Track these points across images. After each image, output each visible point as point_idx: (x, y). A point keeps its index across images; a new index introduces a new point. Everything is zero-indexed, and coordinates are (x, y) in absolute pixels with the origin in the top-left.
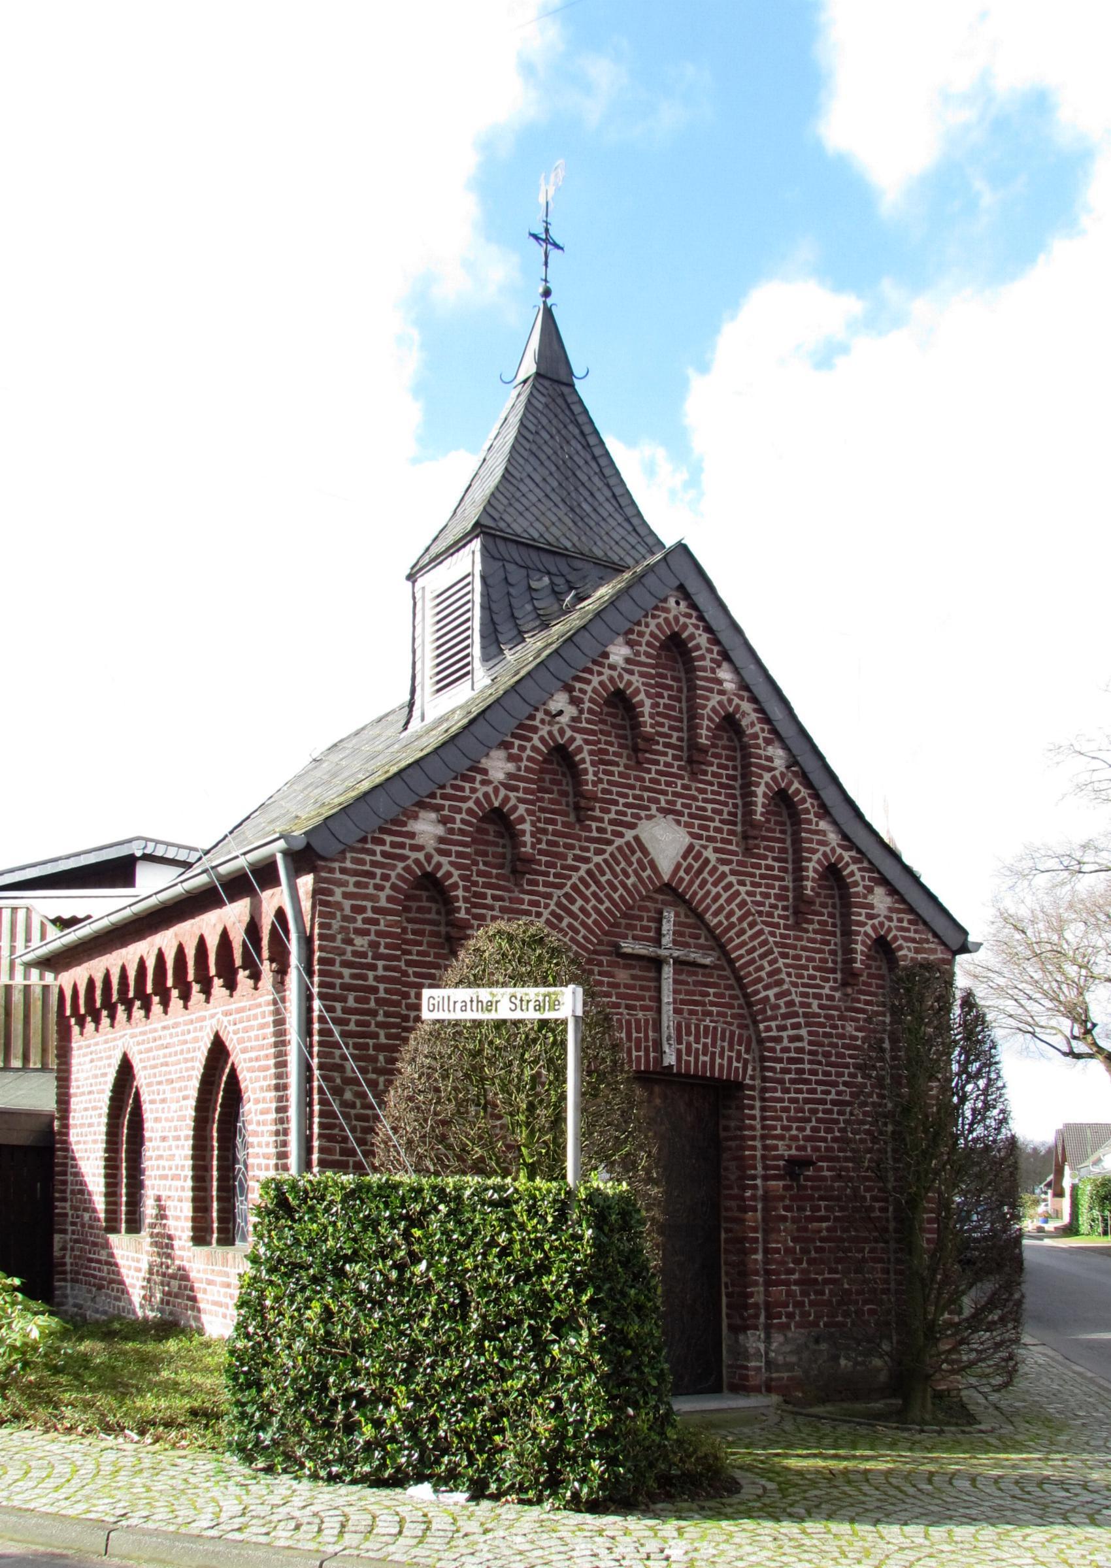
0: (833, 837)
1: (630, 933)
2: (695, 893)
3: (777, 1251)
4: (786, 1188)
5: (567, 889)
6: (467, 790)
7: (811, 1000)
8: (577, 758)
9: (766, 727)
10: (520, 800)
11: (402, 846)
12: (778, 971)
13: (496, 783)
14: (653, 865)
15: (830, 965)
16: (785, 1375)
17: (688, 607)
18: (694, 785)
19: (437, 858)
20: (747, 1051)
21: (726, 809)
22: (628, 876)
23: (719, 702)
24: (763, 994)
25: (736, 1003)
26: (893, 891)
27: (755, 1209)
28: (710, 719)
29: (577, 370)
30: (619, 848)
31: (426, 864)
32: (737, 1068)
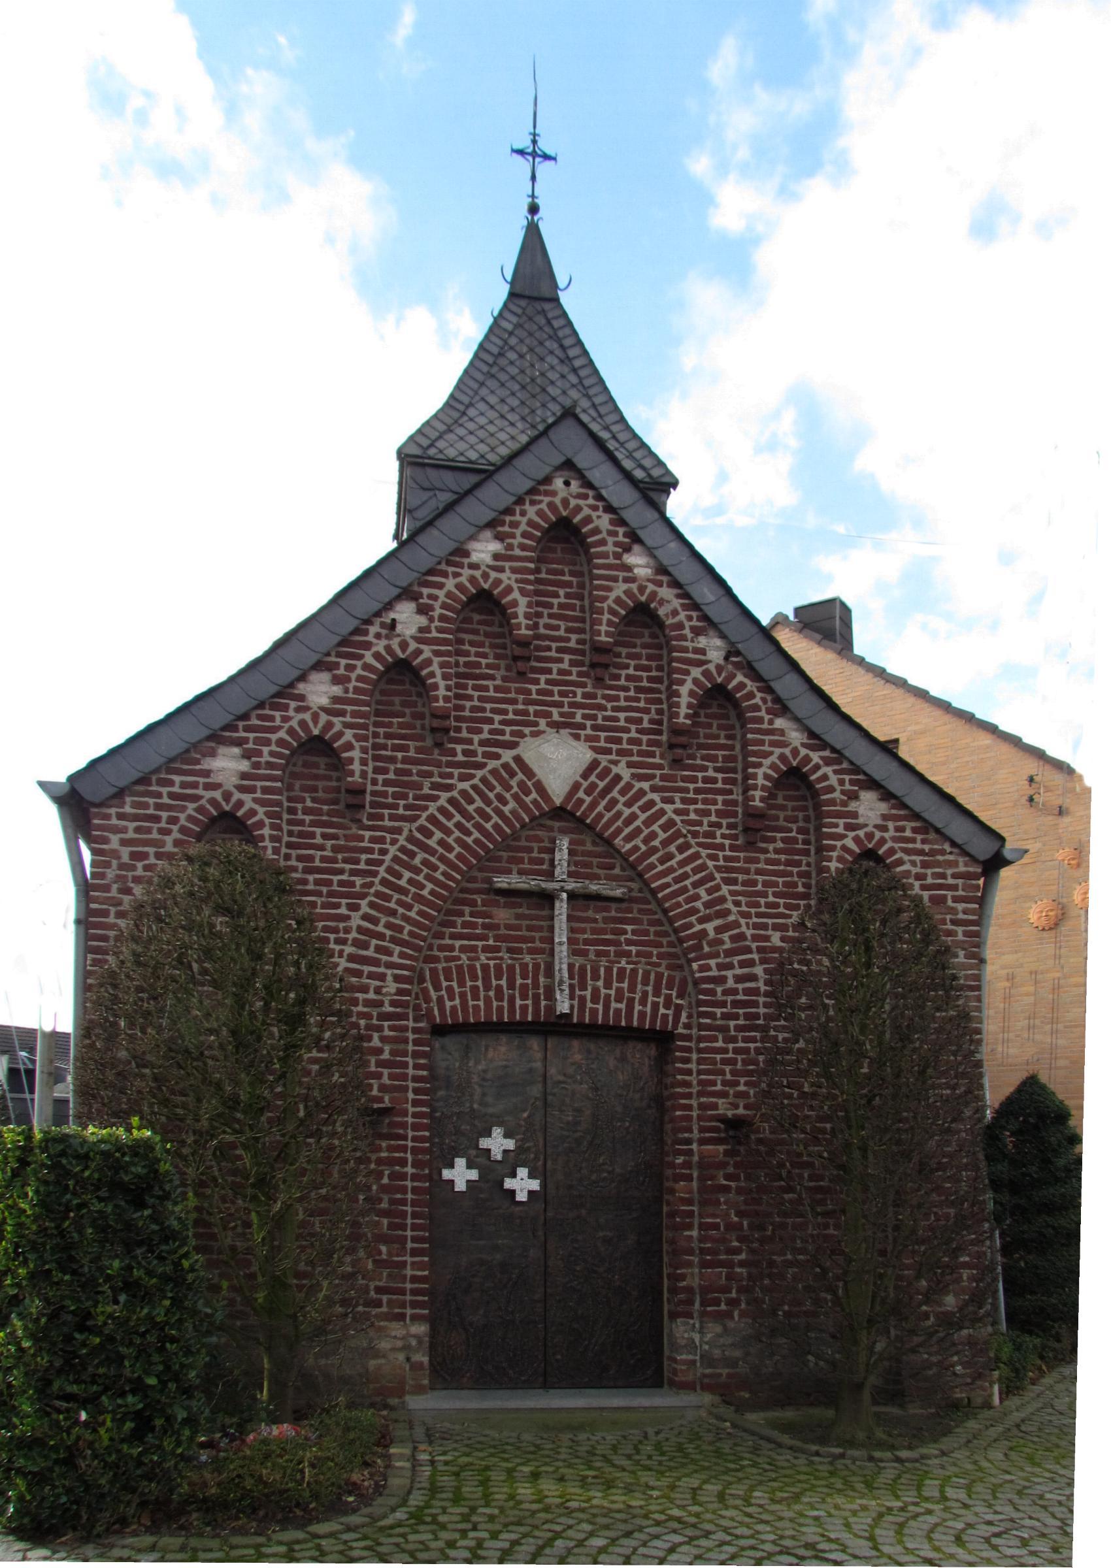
0: (796, 737)
1: (515, 868)
2: (600, 816)
3: (715, 1227)
4: (726, 1152)
5: (422, 821)
6: (278, 719)
7: (770, 932)
8: (424, 673)
9: (694, 614)
10: (347, 725)
11: (195, 785)
12: (723, 900)
13: (315, 709)
14: (540, 788)
15: (801, 889)
16: (725, 1371)
17: (582, 486)
18: (600, 692)
19: (237, 796)
20: (680, 996)
21: (646, 718)
22: (505, 802)
23: (625, 592)
24: (698, 928)
25: (665, 941)
26: (887, 795)
27: (689, 1178)
28: (612, 612)
29: (562, 281)
30: (494, 772)
31: (224, 803)
32: (665, 1016)
